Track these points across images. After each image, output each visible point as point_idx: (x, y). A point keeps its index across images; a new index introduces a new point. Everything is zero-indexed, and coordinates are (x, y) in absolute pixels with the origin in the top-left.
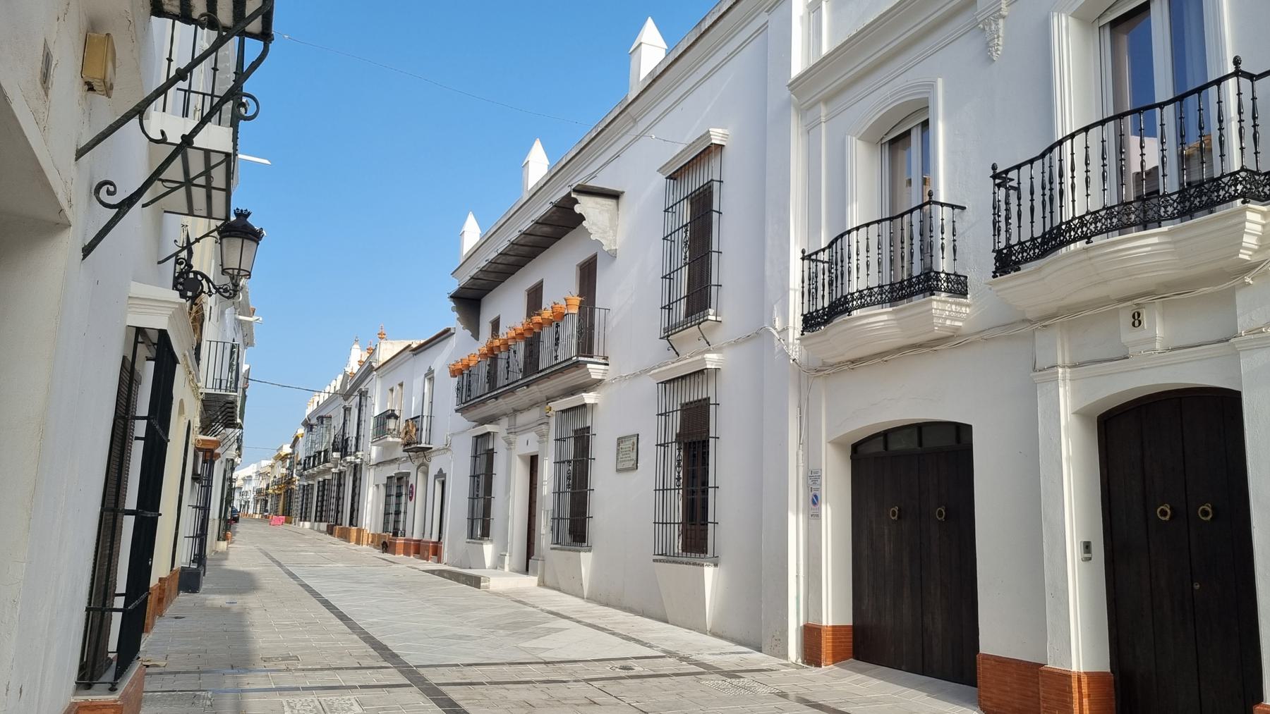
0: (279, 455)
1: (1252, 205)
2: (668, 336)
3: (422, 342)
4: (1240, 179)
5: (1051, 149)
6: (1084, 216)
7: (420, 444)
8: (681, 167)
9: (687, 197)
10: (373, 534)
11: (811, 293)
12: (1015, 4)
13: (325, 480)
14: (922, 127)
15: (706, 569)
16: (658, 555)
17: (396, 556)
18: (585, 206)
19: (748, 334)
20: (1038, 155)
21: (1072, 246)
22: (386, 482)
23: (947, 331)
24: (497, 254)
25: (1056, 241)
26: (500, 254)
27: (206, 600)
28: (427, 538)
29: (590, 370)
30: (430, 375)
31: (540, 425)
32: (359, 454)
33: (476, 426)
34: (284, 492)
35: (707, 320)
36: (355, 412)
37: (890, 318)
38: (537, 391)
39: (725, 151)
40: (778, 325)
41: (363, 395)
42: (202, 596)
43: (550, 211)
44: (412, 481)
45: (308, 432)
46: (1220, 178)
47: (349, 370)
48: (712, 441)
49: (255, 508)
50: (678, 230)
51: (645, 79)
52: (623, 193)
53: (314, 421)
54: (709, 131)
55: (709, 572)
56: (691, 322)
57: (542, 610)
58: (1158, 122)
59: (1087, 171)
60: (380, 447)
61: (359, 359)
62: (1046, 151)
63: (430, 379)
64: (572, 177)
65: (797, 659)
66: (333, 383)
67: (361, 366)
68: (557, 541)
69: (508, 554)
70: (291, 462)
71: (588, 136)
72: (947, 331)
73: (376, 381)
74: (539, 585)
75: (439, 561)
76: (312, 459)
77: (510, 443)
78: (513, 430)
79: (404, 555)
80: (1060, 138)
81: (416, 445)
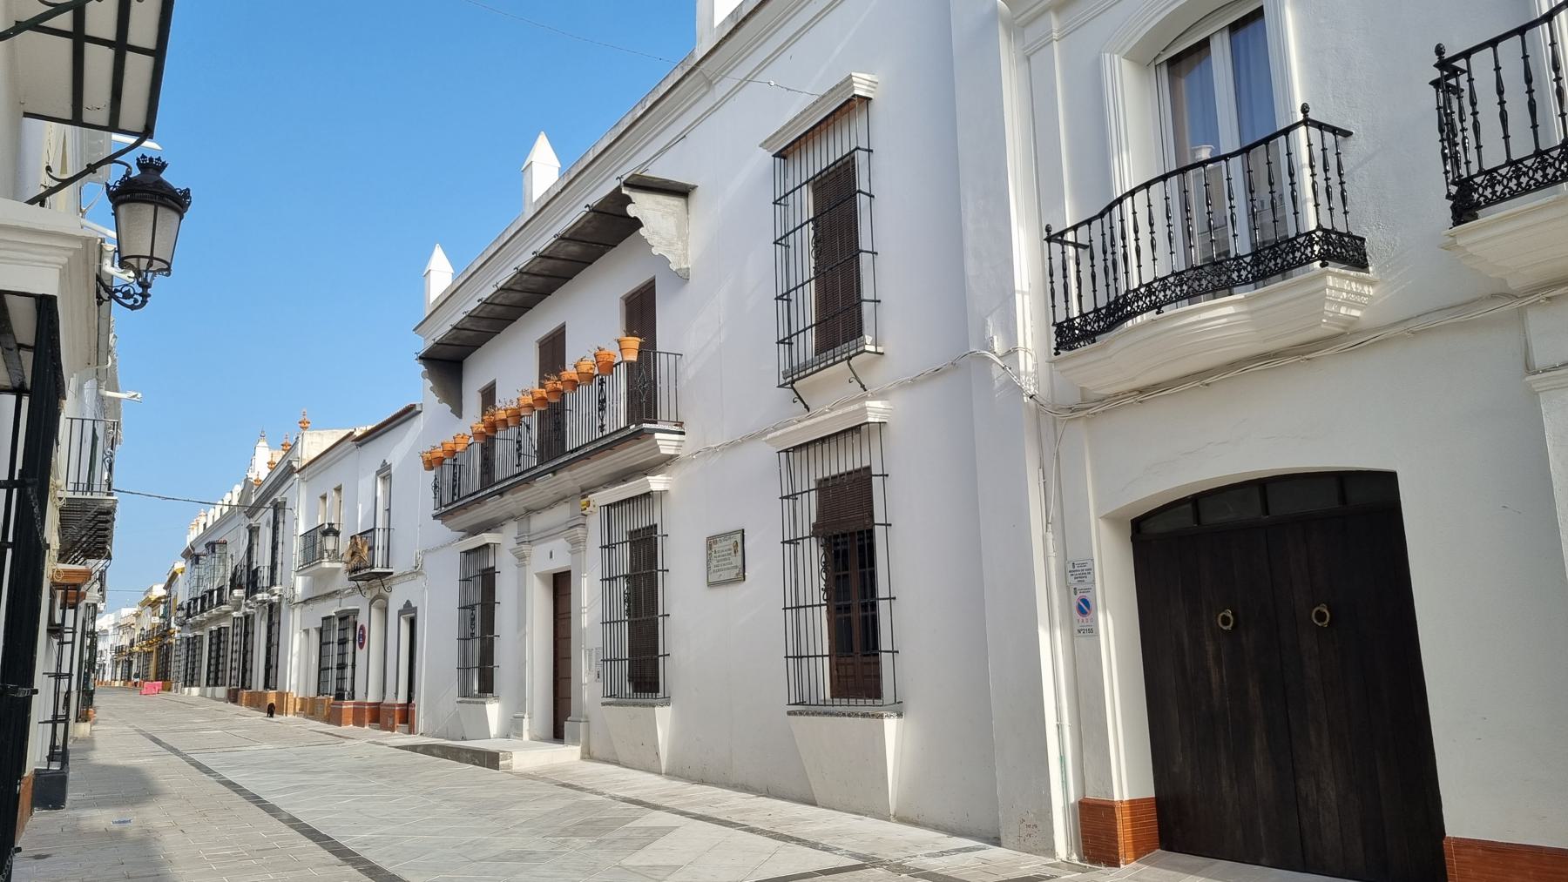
0: (148, 600)
1: (1333, 268)
2: (793, 382)
3: (369, 428)
4: (1317, 239)
5: (1110, 208)
6: (1151, 283)
7: (373, 568)
8: (800, 137)
9: (807, 182)
10: (302, 699)
11: (1053, 294)
12: (1118, 4)
13: (220, 629)
14: (1168, 67)
15: (886, 721)
16: (607, 697)
17: (343, 727)
18: (642, 206)
19: (938, 367)
20: (1097, 214)
21: (1139, 318)
22: (321, 625)
23: (1336, 326)
24: (496, 289)
25: (1114, 317)
26: (502, 289)
27: (78, 819)
28: (389, 699)
29: (659, 442)
30: (385, 473)
31: (571, 527)
32: (277, 589)
33: (463, 537)
34: (157, 649)
35: (864, 351)
36: (266, 535)
37: (1239, 310)
38: (568, 479)
39: (873, 106)
40: (998, 346)
41: (278, 508)
42: (71, 813)
43: (583, 221)
44: (362, 620)
45: (192, 565)
46: (1295, 239)
47: (252, 476)
48: (879, 532)
49: (114, 672)
50: (801, 226)
51: (723, 24)
52: (694, 187)
53: (201, 549)
54: (851, 76)
55: (891, 725)
56: (834, 358)
57: (614, 798)
58: (1225, 177)
59: (1152, 233)
60: (308, 578)
61: (269, 460)
62: (1104, 209)
63: (384, 478)
64: (508, 262)
65: (1069, 855)
66: (228, 497)
67: (272, 469)
68: (613, 697)
69: (526, 716)
70: (165, 608)
71: (630, 116)
72: (1336, 326)
73: (299, 486)
74: (583, 758)
75: (411, 731)
76: (199, 601)
77: (521, 558)
78: (526, 539)
79: (354, 725)
80: (1119, 195)
81: (368, 570)
